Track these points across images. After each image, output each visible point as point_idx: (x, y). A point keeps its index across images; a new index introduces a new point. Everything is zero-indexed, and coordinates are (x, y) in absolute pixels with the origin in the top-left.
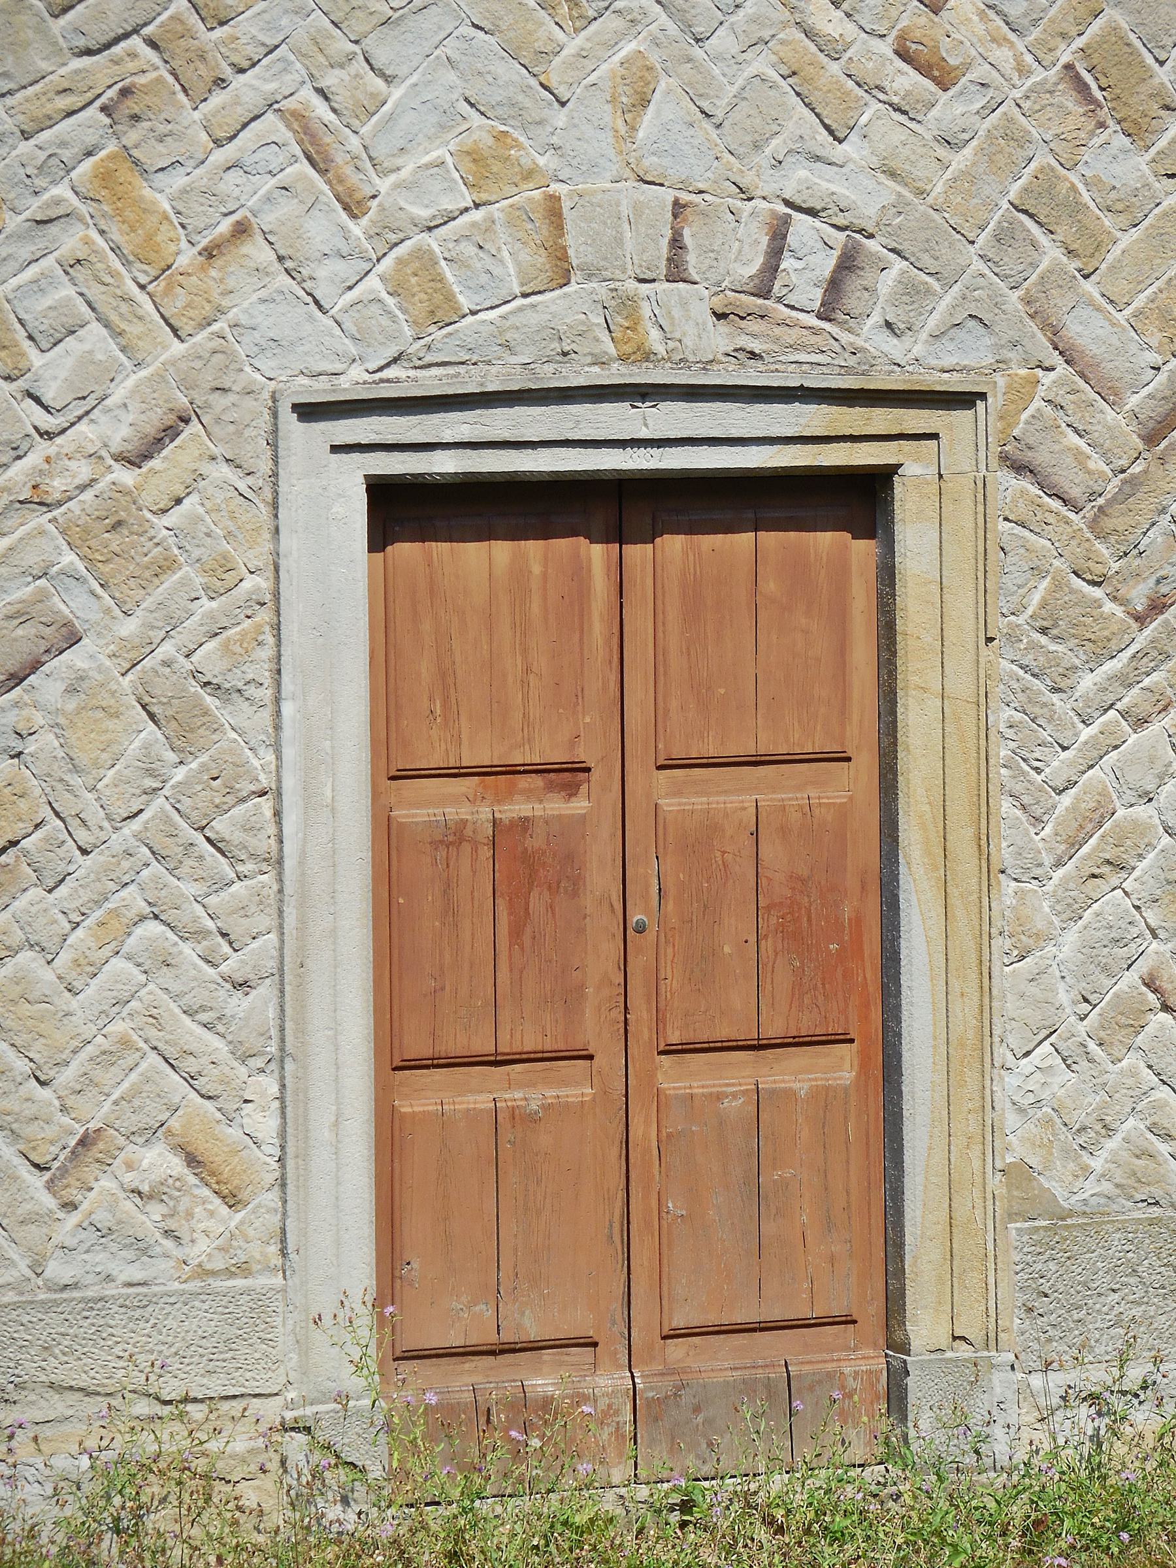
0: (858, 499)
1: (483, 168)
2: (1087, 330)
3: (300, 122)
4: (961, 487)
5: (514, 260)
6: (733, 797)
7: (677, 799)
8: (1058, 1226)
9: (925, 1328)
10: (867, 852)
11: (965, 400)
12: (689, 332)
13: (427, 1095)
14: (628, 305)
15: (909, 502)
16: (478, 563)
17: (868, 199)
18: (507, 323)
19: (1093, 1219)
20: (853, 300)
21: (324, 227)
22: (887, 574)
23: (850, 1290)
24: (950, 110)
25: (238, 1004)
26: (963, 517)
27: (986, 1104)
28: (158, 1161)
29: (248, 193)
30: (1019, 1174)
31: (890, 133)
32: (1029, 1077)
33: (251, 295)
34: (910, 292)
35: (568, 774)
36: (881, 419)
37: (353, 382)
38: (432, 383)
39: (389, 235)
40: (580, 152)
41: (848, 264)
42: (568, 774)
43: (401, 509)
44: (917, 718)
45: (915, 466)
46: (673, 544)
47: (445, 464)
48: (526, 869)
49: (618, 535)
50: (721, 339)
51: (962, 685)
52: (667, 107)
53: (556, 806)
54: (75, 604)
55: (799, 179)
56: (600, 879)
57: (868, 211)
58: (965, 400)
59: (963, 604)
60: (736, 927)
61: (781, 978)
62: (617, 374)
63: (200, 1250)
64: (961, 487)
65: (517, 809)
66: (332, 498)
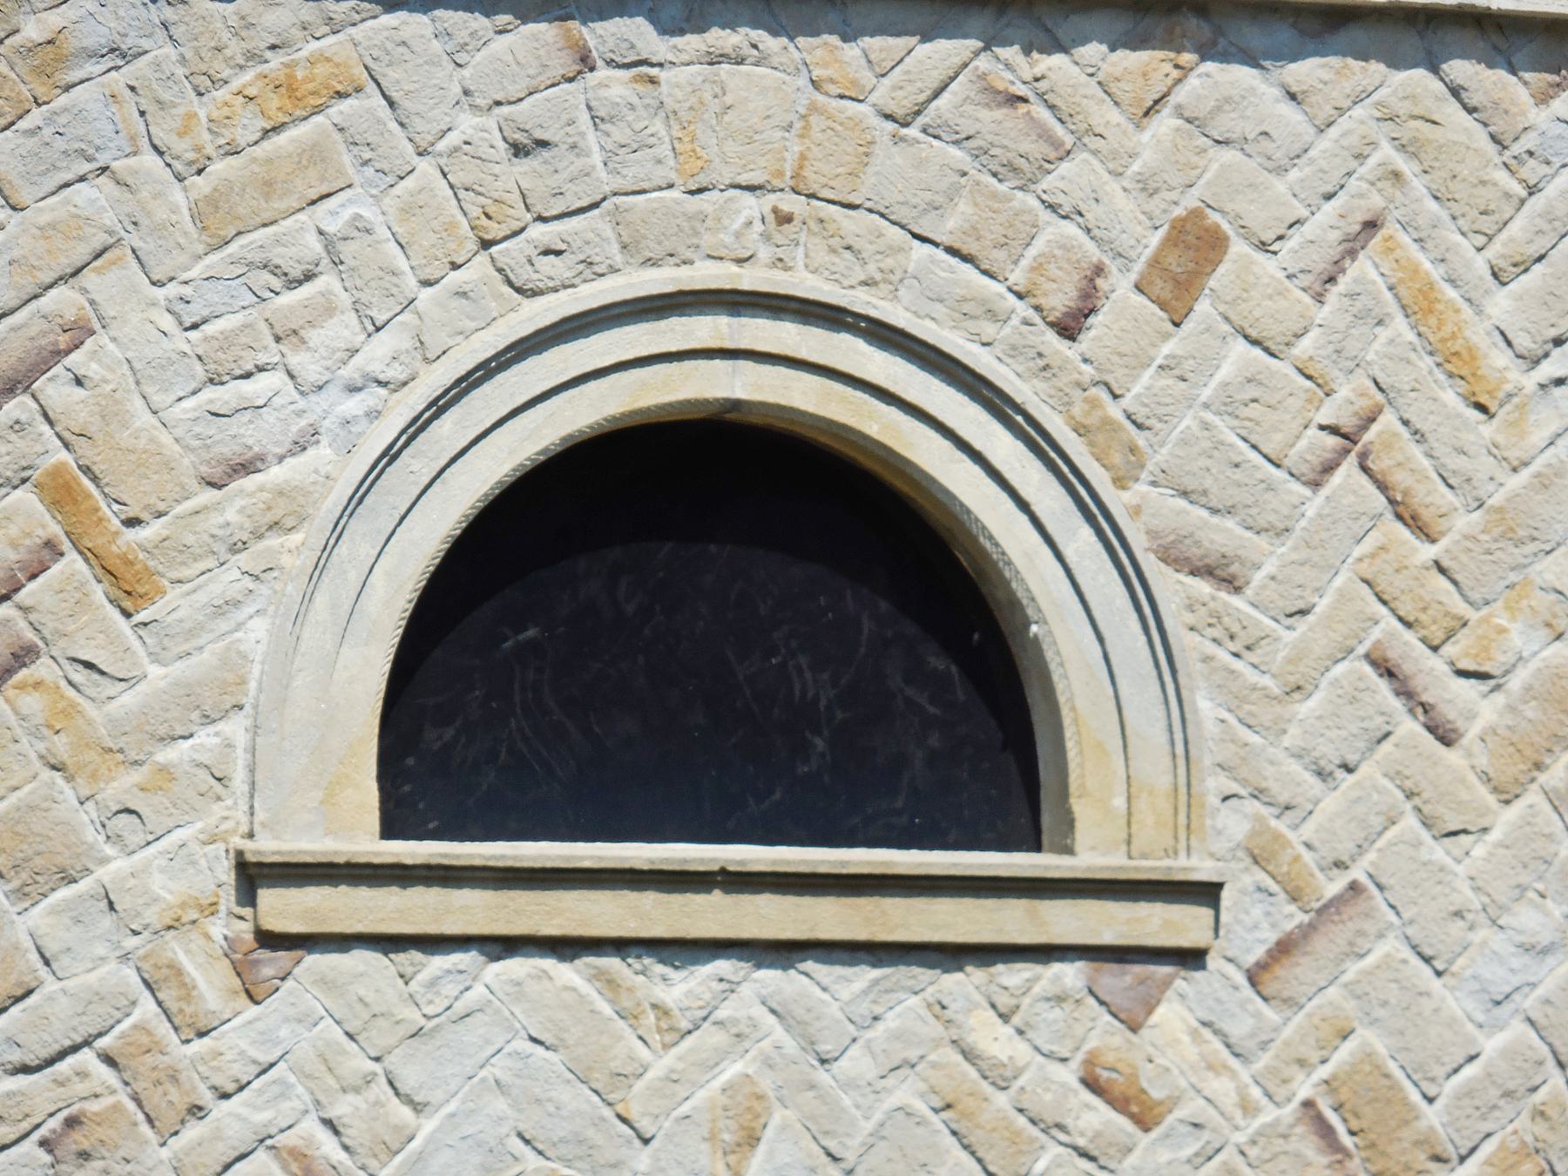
65: (240, 752)
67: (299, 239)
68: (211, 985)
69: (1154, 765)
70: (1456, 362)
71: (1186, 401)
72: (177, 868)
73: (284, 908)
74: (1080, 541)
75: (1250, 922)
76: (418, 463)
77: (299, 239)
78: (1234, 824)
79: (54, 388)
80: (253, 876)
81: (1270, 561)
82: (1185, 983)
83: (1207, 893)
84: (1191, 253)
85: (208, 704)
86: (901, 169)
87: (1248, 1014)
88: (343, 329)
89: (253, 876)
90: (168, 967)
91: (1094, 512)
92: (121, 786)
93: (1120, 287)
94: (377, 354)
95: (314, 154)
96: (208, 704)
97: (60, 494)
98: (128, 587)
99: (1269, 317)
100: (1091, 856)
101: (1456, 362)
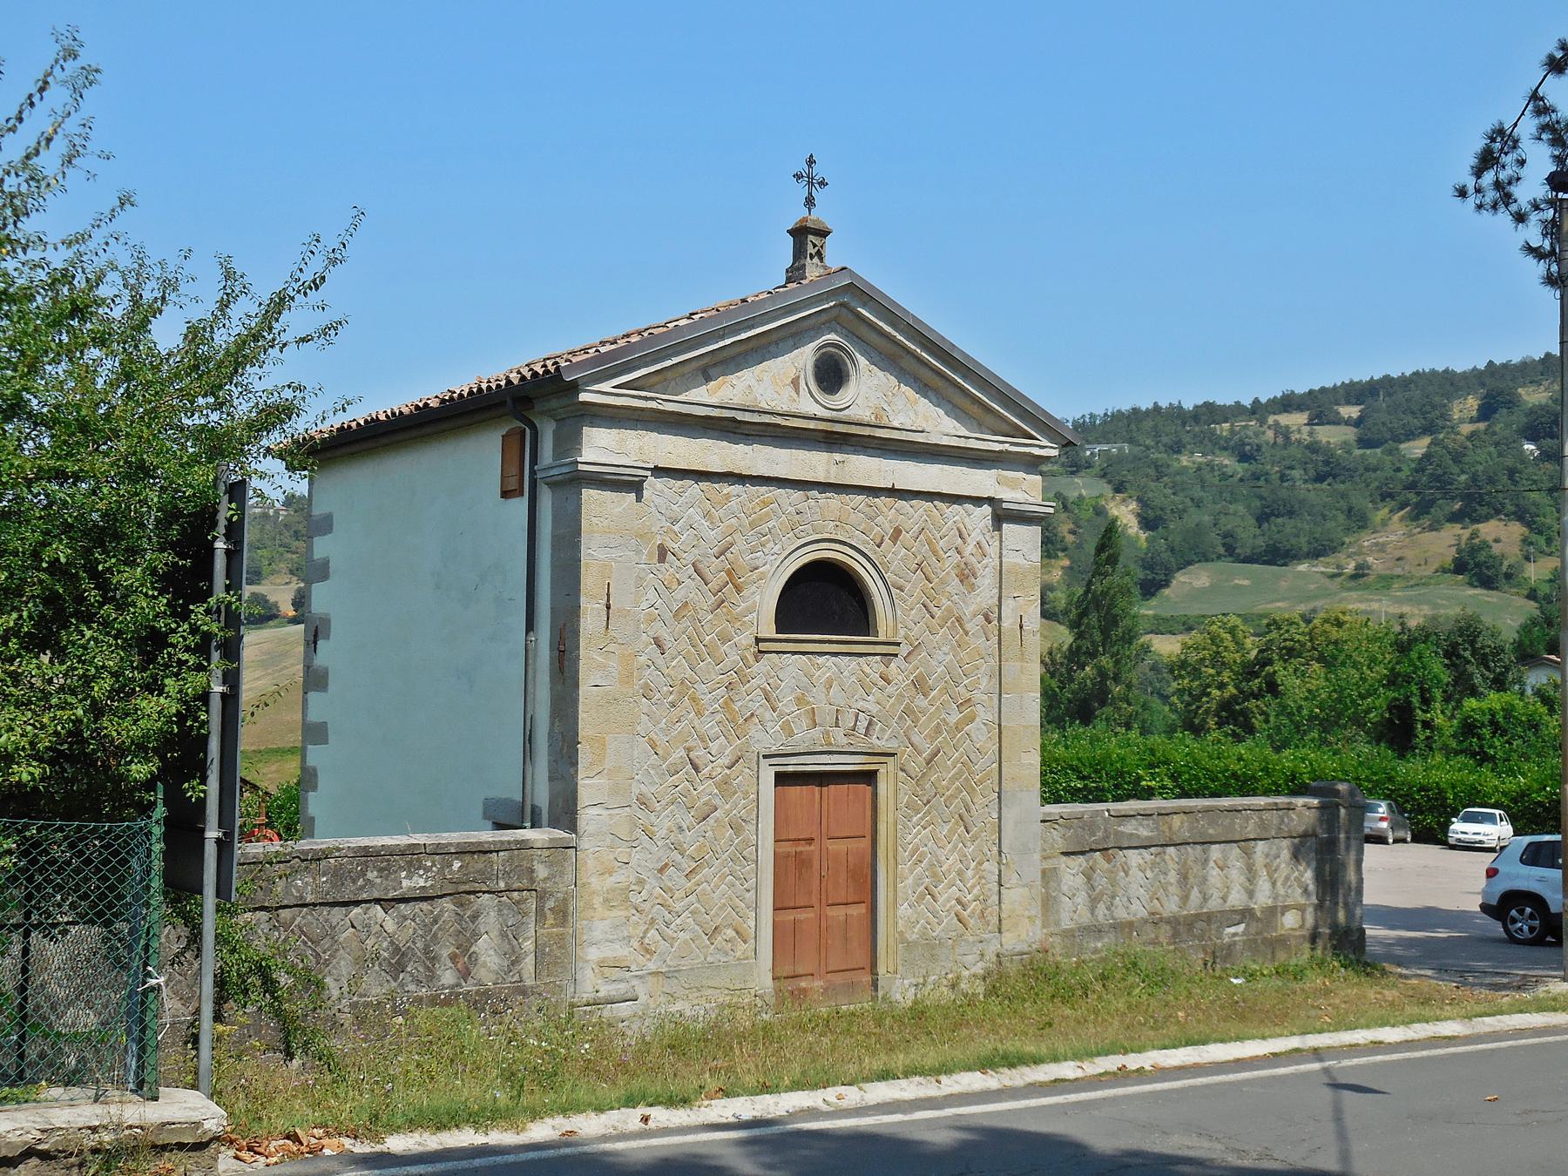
0: (869, 777)
1: (800, 701)
2: (916, 739)
3: (764, 690)
4: (891, 775)
5: (805, 722)
6: (841, 846)
7: (833, 846)
8: (910, 946)
9: (881, 970)
10: (868, 858)
11: (893, 755)
12: (840, 739)
13: (790, 916)
14: (828, 732)
15: (881, 778)
16: (795, 792)
17: (874, 709)
18: (804, 737)
19: (915, 943)
20: (921, 748)
21: (768, 714)
22: (875, 795)
23: (861, 958)
24: (890, 689)
25: (747, 895)
26: (891, 781)
27: (895, 916)
28: (730, 933)
29: (754, 706)
30: (901, 933)
31: (878, 694)
32: (904, 909)
33: (754, 730)
34: (882, 730)
35: (810, 840)
36: (876, 759)
37: (773, 750)
38: (789, 750)
39: (780, 716)
40: (818, 699)
41: (870, 724)
42: (810, 840)
43: (782, 779)
44: (882, 827)
45: (882, 770)
46: (832, 787)
47: (790, 769)
48: (802, 862)
49: (821, 785)
50: (845, 740)
51: (891, 820)
52: (835, 688)
53: (808, 848)
54: (717, 802)
55: (860, 705)
56: (816, 864)
57: (874, 712)
58: (893, 755)
59: (891, 802)
60: (843, 876)
61: (851, 890)
62: (825, 749)
63: (738, 954)
64: (891, 775)
65: (799, 849)
66: (768, 776)
67: (765, 528)
68: (751, 659)
69: (890, 623)
70: (935, 553)
71: (895, 557)
72: (746, 639)
73: (763, 646)
74: (880, 583)
75: (904, 650)
76: (781, 569)
77: (765, 528)
78: (902, 632)
79: (728, 554)
80: (758, 640)
81: (908, 587)
82: (895, 659)
83: (898, 644)
84: (897, 532)
85: (750, 611)
86: (854, 518)
87: (904, 665)
88: (771, 544)
89: (758, 640)
90: (1493, 140)
91: (882, 578)
92: (738, 625)
93: (886, 539)
94: (776, 549)
95: (767, 514)
96: (750, 611)
97: (729, 573)
98: (738, 589)
99: (907, 544)
100: (881, 638)
101: (935, 553)
